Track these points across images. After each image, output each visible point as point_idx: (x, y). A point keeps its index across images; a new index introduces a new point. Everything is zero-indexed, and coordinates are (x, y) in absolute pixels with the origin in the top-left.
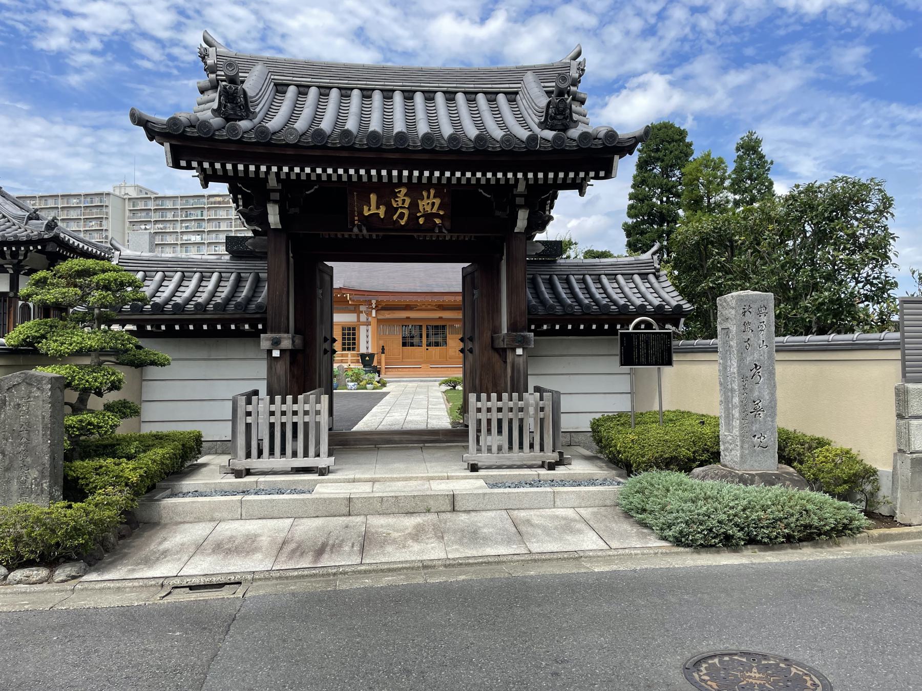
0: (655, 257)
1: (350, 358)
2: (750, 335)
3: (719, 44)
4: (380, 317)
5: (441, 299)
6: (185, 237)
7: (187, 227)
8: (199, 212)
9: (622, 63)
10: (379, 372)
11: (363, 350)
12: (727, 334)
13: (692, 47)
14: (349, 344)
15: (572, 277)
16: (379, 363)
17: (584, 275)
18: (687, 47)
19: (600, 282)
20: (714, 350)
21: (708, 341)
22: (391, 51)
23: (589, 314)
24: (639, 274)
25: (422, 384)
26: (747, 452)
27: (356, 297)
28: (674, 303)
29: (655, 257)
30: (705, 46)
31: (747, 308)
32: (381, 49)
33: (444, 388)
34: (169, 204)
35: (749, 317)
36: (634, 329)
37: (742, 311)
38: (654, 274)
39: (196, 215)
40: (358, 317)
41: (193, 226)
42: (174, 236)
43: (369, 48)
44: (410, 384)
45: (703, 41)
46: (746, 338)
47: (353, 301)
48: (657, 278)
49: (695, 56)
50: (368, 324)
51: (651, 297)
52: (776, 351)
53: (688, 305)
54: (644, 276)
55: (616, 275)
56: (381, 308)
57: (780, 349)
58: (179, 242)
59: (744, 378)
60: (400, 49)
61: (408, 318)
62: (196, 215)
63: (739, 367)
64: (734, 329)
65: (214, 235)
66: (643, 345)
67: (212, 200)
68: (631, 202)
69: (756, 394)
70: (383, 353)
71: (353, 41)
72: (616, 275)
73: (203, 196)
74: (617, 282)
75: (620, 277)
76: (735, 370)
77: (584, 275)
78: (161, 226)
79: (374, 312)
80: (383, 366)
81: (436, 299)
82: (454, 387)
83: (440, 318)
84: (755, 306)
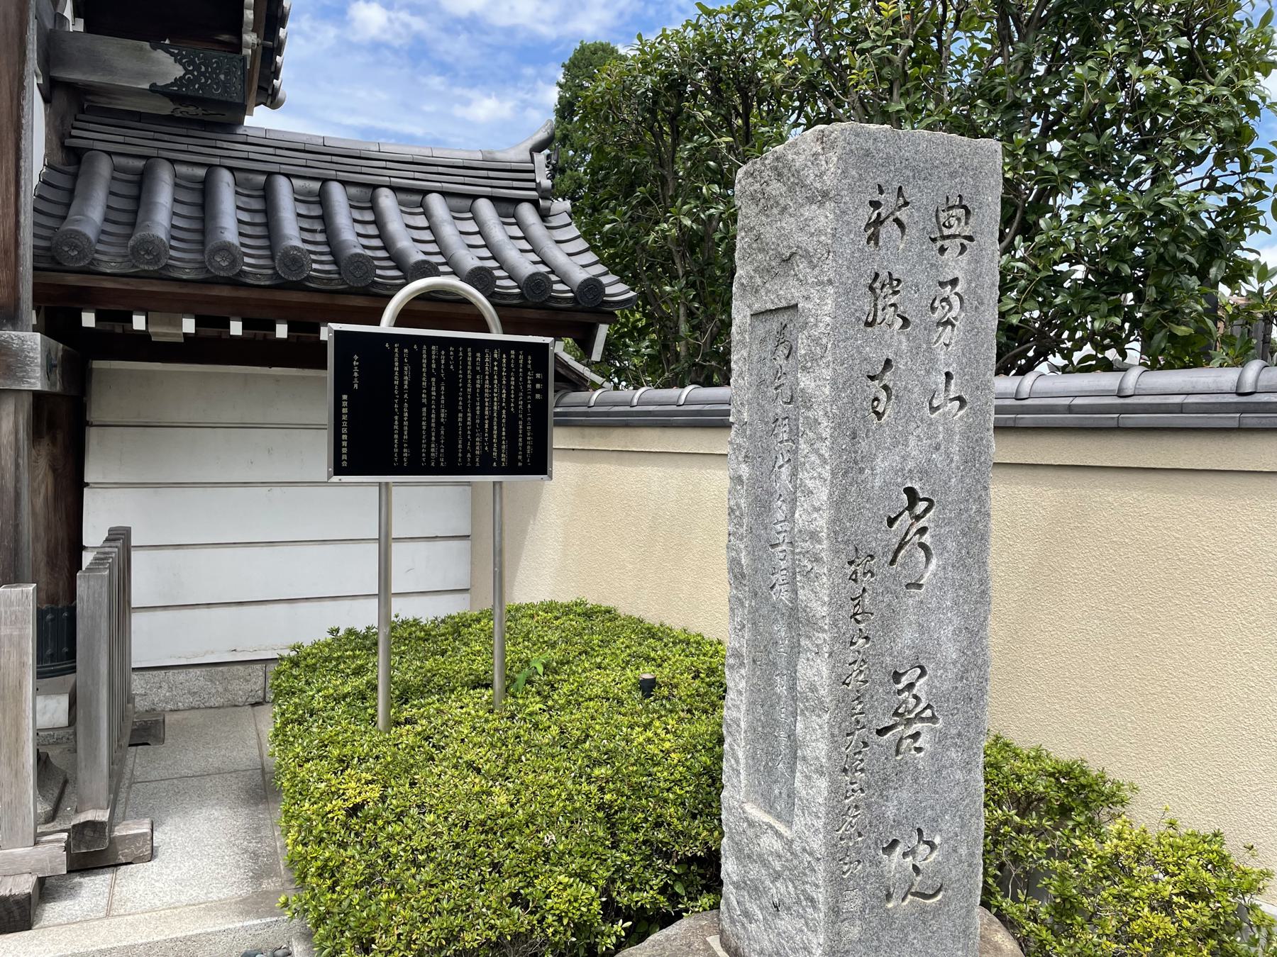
0: (540, 158)
2: (895, 341)
12: (784, 340)
13: (658, 12)
15: (283, 186)
17: (324, 181)
19: (373, 206)
20: (716, 421)
21: (674, 392)
23: (299, 286)
24: (493, 199)
26: (855, 932)
28: (580, 276)
29: (540, 158)
31: (889, 199)
35: (898, 255)
36: (401, 320)
37: (867, 214)
38: (535, 203)
46: (877, 356)
48: (544, 215)
51: (512, 253)
52: (998, 429)
53: (622, 287)
54: (506, 206)
55: (425, 192)
57: (1013, 423)
59: (857, 560)
63: (838, 503)
64: (822, 308)
66: (432, 390)
69: (908, 636)
72: (425, 192)
74: (427, 214)
75: (435, 201)
76: (821, 522)
77: (324, 181)
84: (923, 197)
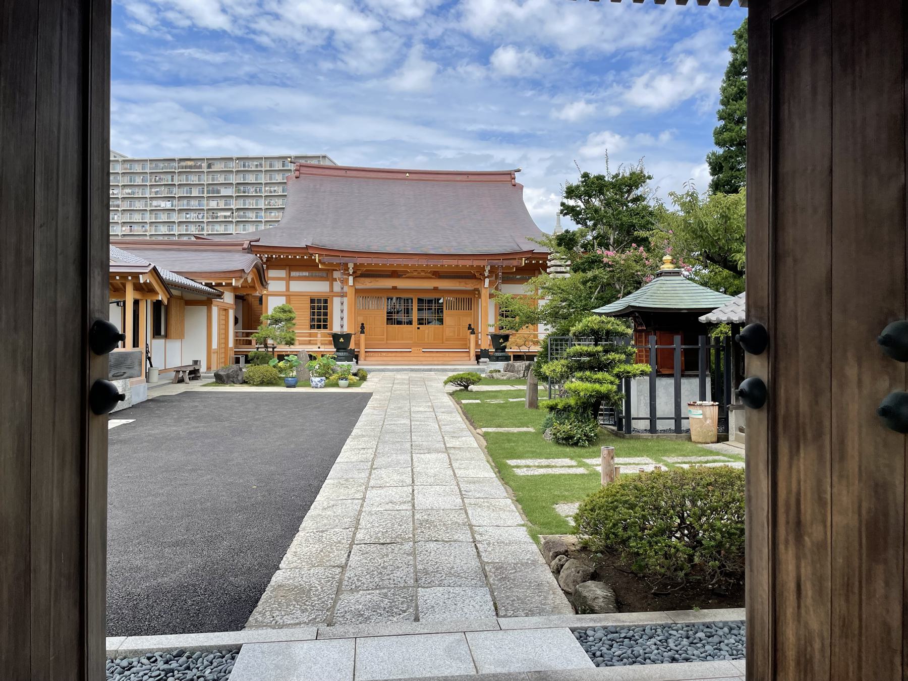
1: (319, 338)
3: (721, 18)
4: (359, 286)
5: (439, 263)
6: (155, 203)
7: (156, 193)
8: (170, 177)
9: (622, 36)
10: (357, 357)
11: (336, 329)
13: (693, 21)
14: (319, 320)
16: (358, 344)
18: (688, 21)
22: (390, 18)
25: (414, 375)
27: (326, 260)
30: (707, 21)
32: (379, 17)
33: (452, 388)
34: (138, 168)
39: (167, 179)
40: (331, 286)
41: (164, 192)
42: (143, 202)
43: (368, 16)
44: (399, 376)
45: (705, 15)
47: (323, 264)
49: (696, 31)
50: (343, 295)
56: (362, 273)
58: (148, 209)
60: (398, 17)
61: (395, 288)
62: (167, 179)
65: (185, 202)
67: (183, 164)
68: (722, 123)
70: (362, 332)
71: (352, 9)
73: (174, 160)
78: (128, 191)
79: (351, 278)
80: (363, 350)
81: (432, 263)
82: (466, 387)
83: (436, 289)
